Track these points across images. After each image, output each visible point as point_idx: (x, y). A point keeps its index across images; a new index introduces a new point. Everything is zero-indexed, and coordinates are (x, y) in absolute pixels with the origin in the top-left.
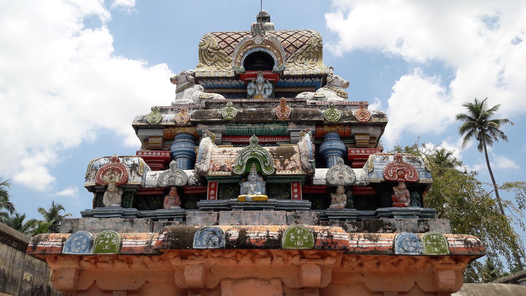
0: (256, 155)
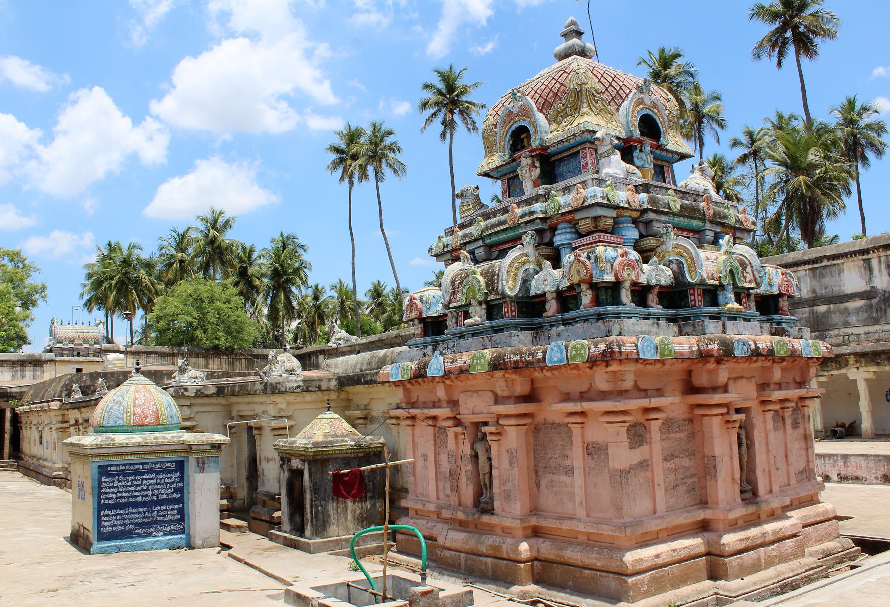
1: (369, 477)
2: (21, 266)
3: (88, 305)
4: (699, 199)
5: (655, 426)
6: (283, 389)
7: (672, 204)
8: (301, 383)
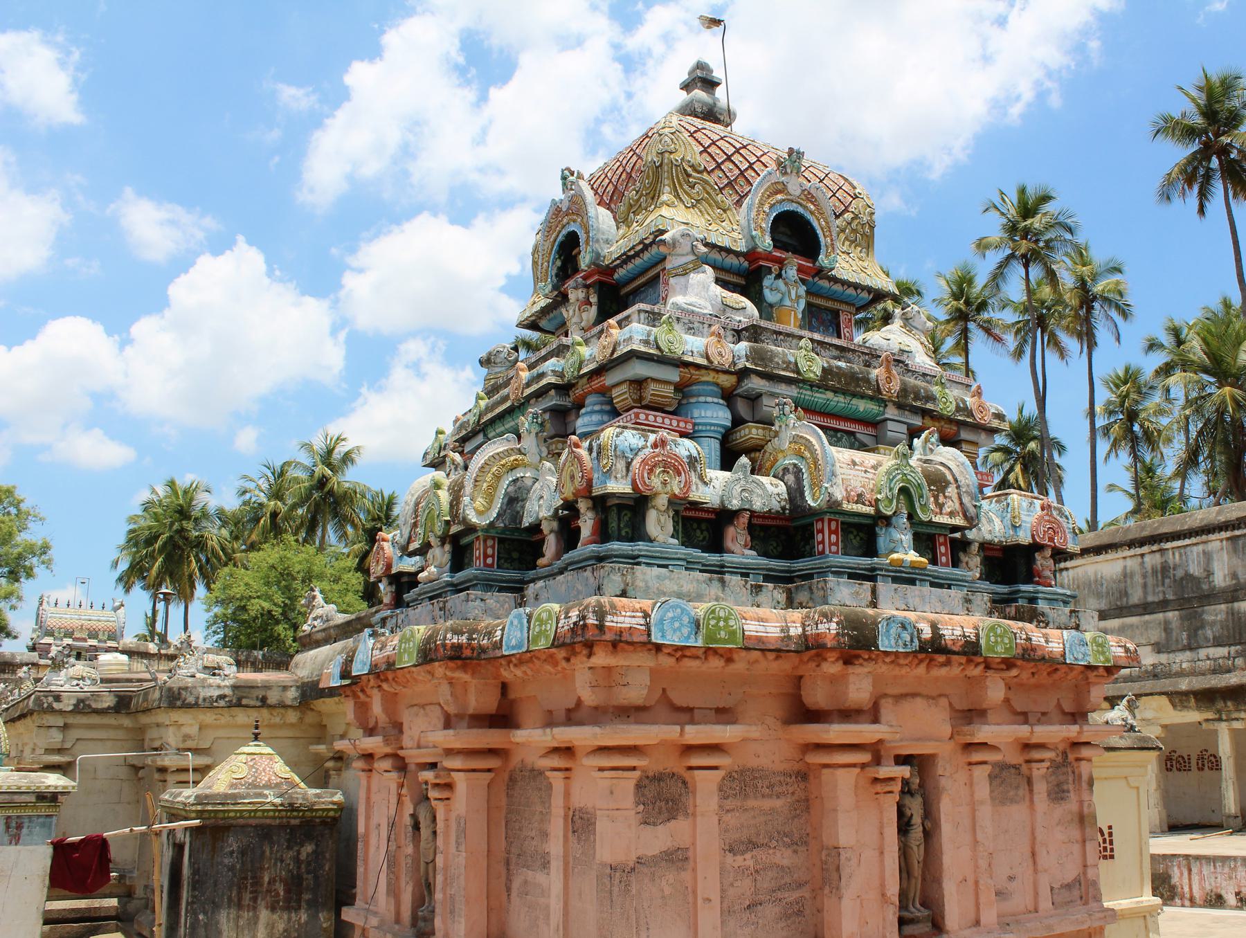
0: (909, 481)
1: (309, 864)
2: (13, 511)
3: (126, 581)
4: (875, 363)
5: (706, 785)
6: (191, 700)
7: (803, 365)
8: (228, 692)
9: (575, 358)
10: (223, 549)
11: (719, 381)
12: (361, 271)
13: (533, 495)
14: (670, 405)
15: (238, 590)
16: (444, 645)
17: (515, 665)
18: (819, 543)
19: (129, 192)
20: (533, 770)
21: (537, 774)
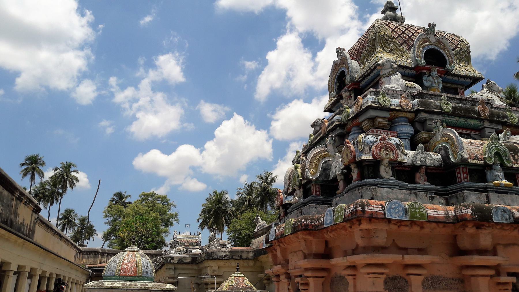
0: (499, 149)
2: (166, 204)
3: (202, 226)
6: (215, 257)
7: (444, 106)
8: (228, 254)
9: (346, 113)
10: (233, 213)
11: (407, 116)
12: (277, 120)
13: (333, 167)
14: (387, 127)
15: (238, 227)
16: (301, 224)
17: (330, 232)
18: (458, 178)
19: (202, 101)
20: (340, 277)
21: (342, 278)
